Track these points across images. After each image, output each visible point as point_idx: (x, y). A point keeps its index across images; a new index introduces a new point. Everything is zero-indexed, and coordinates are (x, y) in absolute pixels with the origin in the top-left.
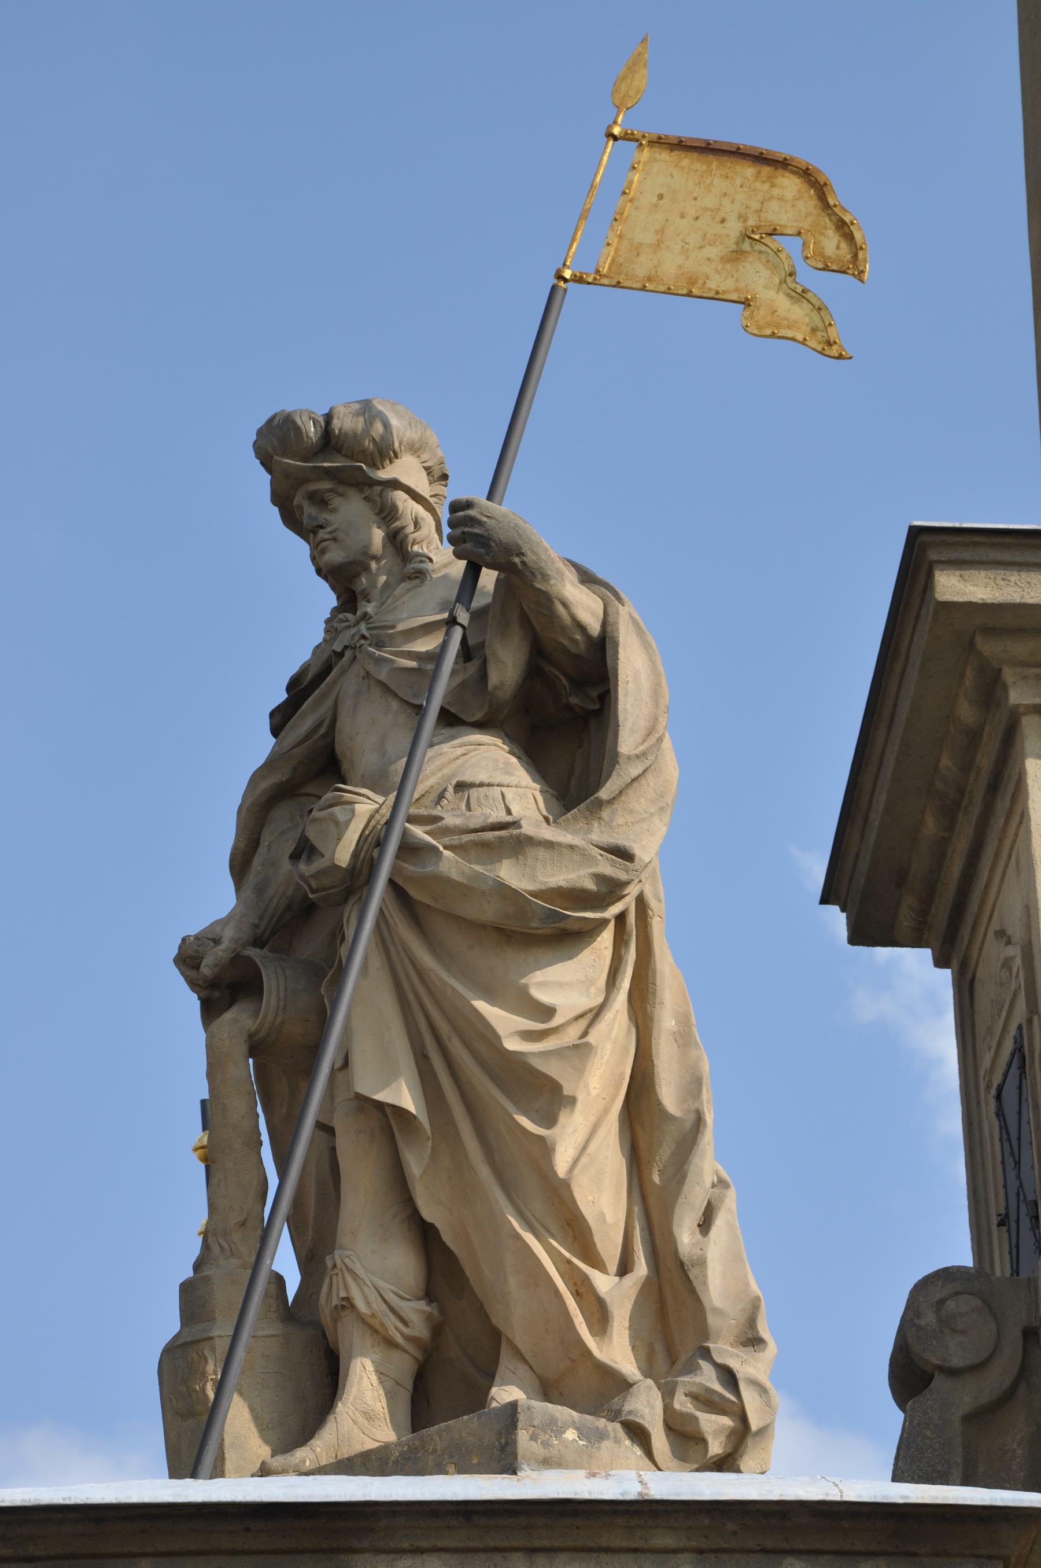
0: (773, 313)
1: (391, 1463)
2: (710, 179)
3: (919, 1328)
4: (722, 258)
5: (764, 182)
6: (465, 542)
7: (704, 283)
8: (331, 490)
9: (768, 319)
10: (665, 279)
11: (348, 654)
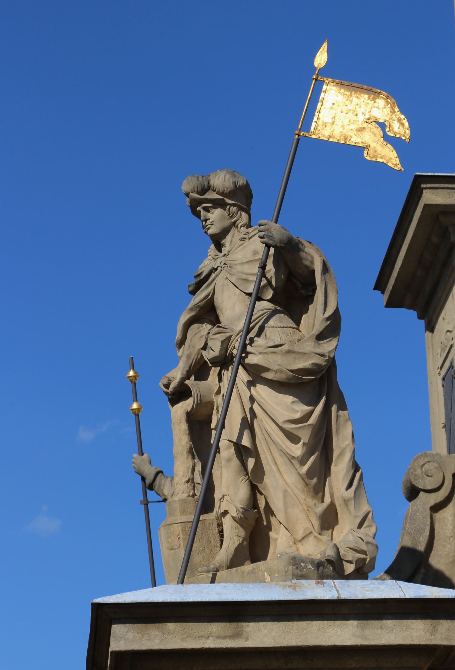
0: (376, 152)
1: (246, 573)
2: (351, 98)
3: (415, 475)
4: (357, 130)
5: (371, 101)
6: (265, 238)
7: (350, 139)
8: (211, 207)
9: (374, 154)
10: (336, 136)
11: (219, 269)
